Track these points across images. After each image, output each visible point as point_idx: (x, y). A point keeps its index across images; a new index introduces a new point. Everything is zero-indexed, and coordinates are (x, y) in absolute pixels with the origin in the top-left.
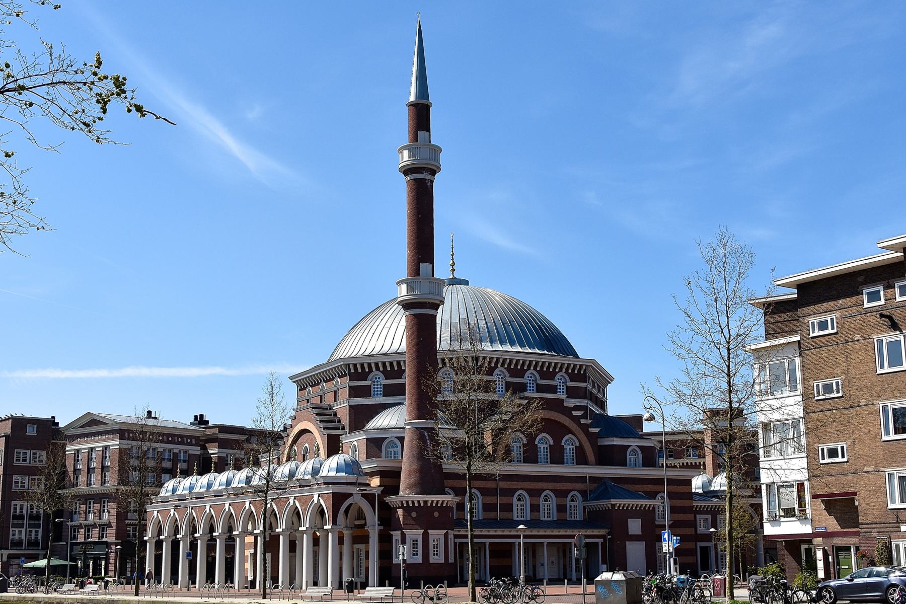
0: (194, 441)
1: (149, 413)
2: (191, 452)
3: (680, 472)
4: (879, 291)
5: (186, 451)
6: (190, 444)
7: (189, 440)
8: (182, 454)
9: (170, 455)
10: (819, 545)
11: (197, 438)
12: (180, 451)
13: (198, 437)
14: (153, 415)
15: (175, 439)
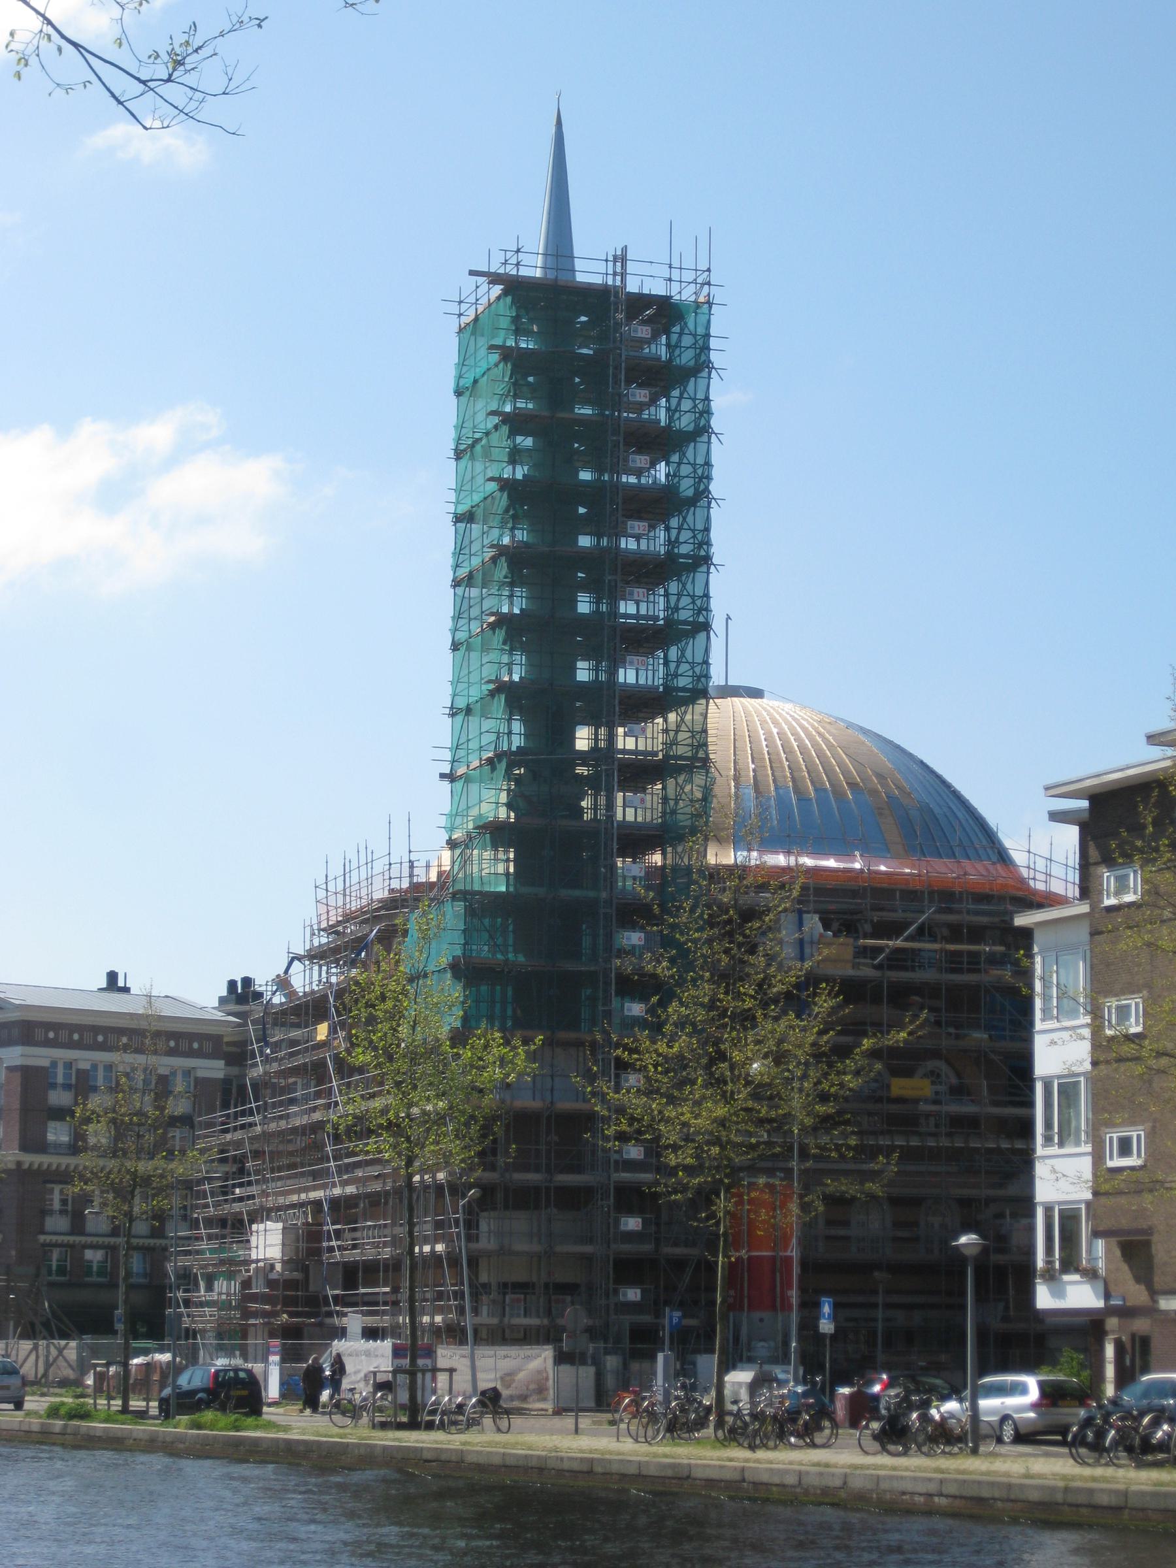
0: (39, 1034)
1: (112, 977)
2: (201, 1074)
3: (369, 1168)
4: (1129, 875)
5: (189, 1072)
6: (199, 1054)
7: (196, 1045)
8: (179, 1078)
9: (67, 1076)
10: (1113, 1332)
11: (216, 1039)
12: (174, 1074)
13: (220, 1037)
14: (121, 983)
15: (64, 1035)
